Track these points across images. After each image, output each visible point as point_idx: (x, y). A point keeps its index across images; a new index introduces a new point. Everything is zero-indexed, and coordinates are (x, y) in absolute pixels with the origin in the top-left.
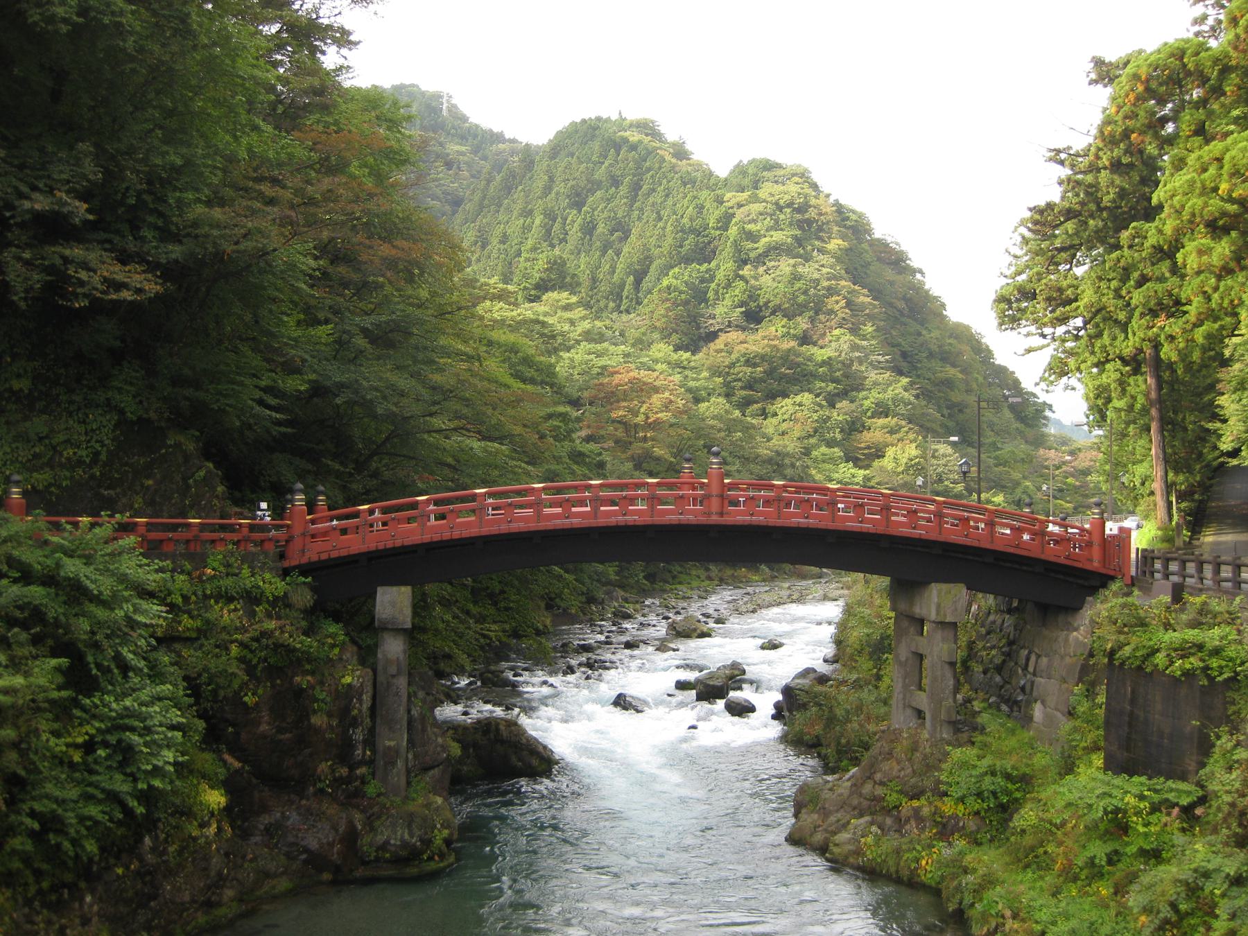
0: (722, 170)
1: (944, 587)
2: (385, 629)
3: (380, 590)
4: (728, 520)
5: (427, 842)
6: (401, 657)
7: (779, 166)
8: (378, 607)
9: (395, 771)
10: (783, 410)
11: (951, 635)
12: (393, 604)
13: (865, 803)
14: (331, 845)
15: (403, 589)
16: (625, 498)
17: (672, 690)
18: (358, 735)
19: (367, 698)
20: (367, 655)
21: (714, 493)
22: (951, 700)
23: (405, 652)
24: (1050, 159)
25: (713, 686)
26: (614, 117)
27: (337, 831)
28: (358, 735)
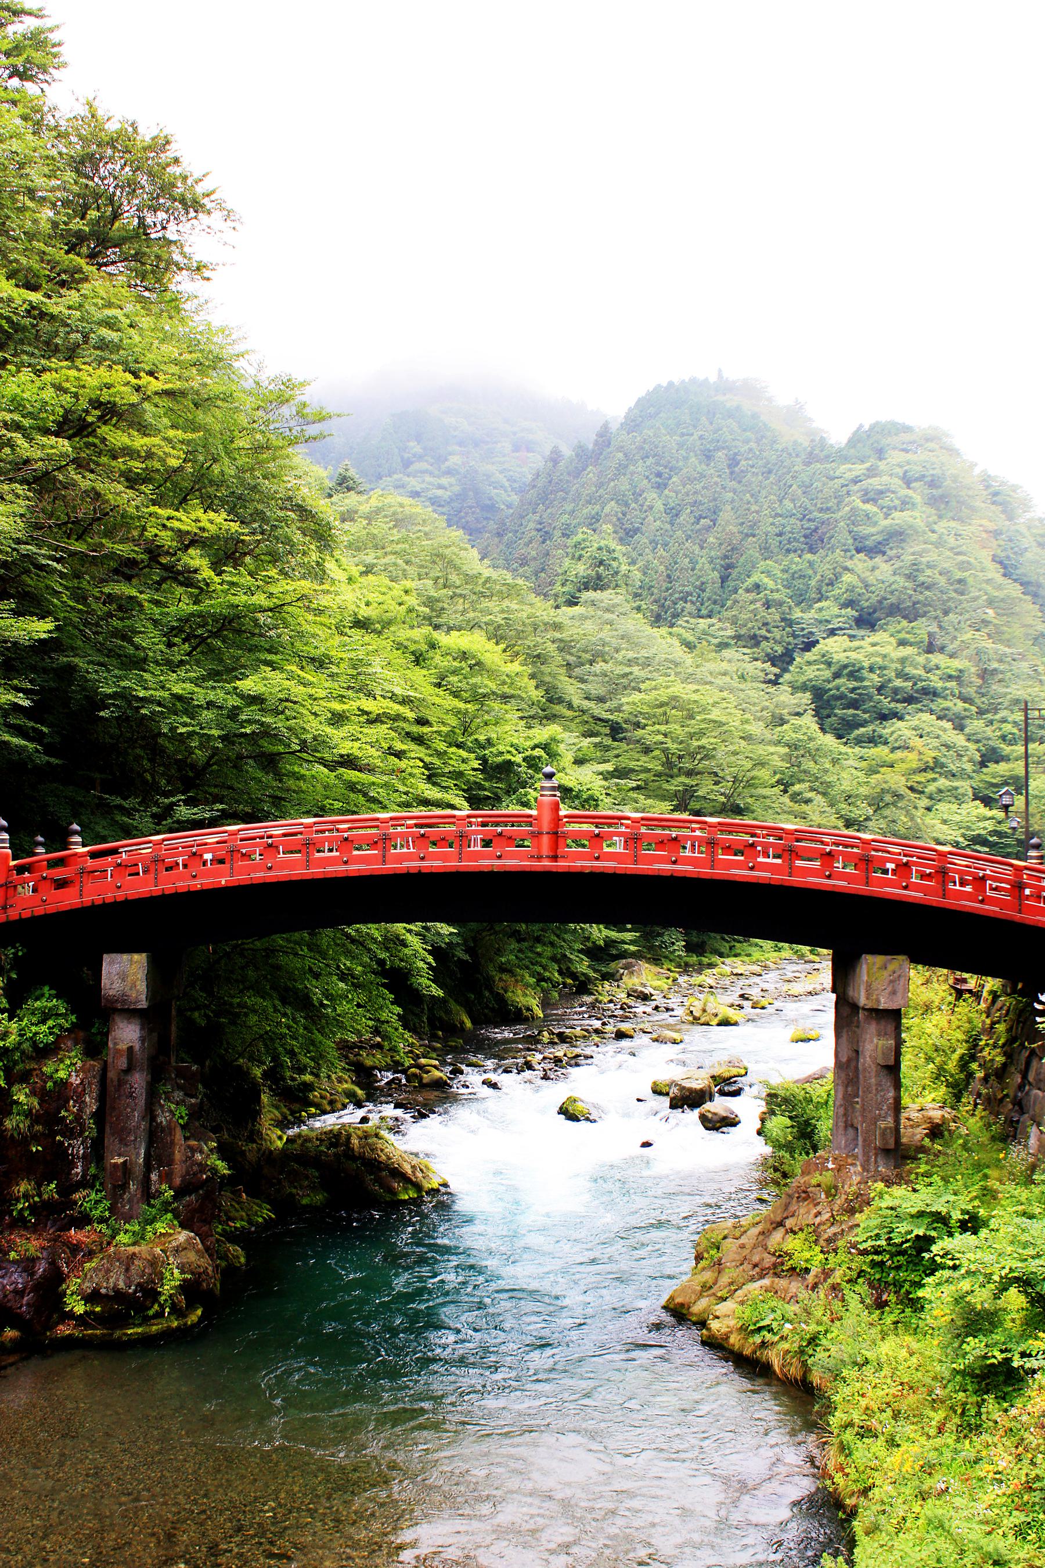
0: (838, 436)
1: (879, 959)
2: (116, 1010)
3: (144, 955)
4: (562, 865)
5: (152, 1294)
6: (137, 1046)
7: (907, 429)
8: (105, 981)
9: (126, 1196)
10: (895, 735)
11: (890, 1028)
12: (123, 977)
13: (769, 1260)
14: (19, 1293)
15: (136, 957)
16: (500, 834)
17: (647, 1092)
18: (78, 1148)
19: (91, 1104)
20: (94, 1048)
21: (545, 830)
22: (890, 1119)
23: (142, 1039)
24: (193, 205)
25: (690, 1090)
26: (713, 378)
27: (32, 1274)
28: (78, 1148)
